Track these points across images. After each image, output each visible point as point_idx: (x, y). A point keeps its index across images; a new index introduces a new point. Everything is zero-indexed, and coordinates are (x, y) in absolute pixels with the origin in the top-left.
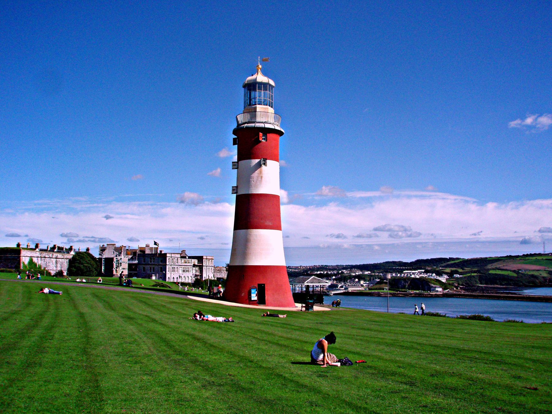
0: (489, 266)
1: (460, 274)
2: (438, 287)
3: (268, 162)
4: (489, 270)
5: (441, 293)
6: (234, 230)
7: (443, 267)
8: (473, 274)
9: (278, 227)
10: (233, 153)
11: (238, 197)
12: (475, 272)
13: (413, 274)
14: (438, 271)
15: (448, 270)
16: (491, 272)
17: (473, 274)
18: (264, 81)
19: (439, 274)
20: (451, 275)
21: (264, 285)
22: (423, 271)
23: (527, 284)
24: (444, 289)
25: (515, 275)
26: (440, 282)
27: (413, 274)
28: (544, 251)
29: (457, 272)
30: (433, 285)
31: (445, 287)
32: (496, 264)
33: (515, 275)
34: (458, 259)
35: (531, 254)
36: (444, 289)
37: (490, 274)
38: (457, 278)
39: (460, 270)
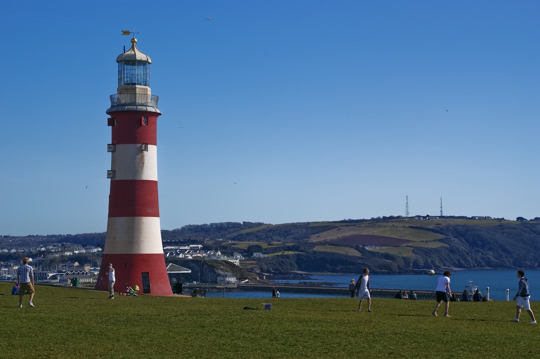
0: (314, 239)
1: (266, 251)
2: (231, 277)
3: (149, 146)
4: (313, 245)
5: (236, 286)
6: (110, 216)
7: (233, 239)
8: (286, 253)
9: (157, 215)
10: (106, 134)
11: (112, 182)
12: (289, 249)
13: (183, 251)
14: (225, 248)
15: (244, 245)
16: (316, 249)
17: (286, 253)
18: (143, 59)
19: (229, 251)
20: (248, 253)
21: (148, 273)
22: (200, 246)
23: (378, 270)
24: (240, 279)
25: (358, 254)
26: (232, 265)
27: (183, 251)
28: (408, 213)
29: (258, 249)
30: (220, 272)
31: (242, 275)
32: (324, 233)
33: (358, 254)
34: (260, 224)
35: (384, 218)
36: (240, 279)
37: (315, 253)
38: (259, 259)
39: (264, 245)
